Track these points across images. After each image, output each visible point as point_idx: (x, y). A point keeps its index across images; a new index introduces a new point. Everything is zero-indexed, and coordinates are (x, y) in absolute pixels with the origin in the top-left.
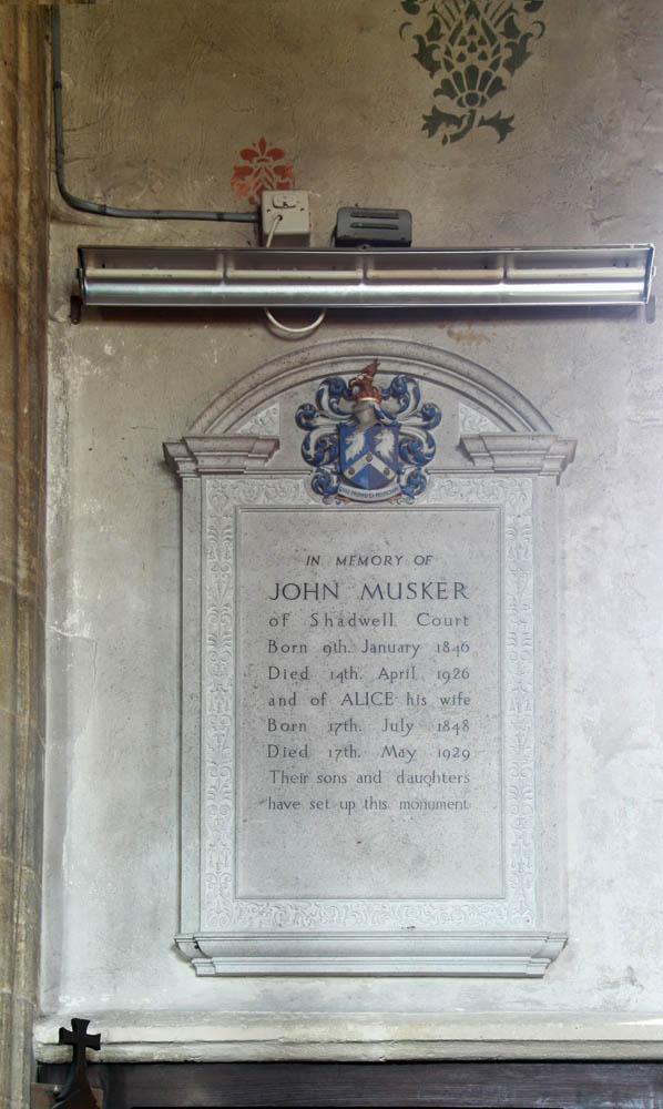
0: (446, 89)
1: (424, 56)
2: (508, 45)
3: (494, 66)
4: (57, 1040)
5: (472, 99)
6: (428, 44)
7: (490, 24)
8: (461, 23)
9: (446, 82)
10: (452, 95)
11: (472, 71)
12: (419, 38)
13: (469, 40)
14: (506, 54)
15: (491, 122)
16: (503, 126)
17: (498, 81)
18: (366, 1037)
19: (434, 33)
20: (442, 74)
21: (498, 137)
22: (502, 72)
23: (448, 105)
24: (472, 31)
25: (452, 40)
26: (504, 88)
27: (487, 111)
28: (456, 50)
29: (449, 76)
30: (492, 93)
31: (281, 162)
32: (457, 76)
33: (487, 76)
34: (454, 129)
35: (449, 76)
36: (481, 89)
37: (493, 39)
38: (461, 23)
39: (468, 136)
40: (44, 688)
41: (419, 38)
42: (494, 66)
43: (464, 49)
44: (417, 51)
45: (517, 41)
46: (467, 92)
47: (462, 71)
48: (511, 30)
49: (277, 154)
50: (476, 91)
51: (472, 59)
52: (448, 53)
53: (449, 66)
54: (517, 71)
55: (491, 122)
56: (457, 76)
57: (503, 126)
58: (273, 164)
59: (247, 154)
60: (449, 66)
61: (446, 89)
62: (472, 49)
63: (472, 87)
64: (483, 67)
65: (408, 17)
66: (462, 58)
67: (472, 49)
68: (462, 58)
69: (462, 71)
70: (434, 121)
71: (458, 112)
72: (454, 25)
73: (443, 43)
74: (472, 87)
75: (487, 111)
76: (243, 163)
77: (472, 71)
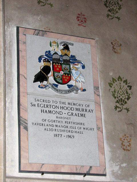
0: (117, 102)
2: (127, 95)
4: (20, 28)
6: (114, 93)
7: (124, 91)
8: (119, 90)
9: (109, 10)
11: (121, 99)
13: (120, 93)
14: (127, 97)
15: (117, 18)
17: (126, 101)
18: (81, 85)
19: (115, 92)
21: (127, 112)
23: (118, 105)
24: (121, 92)
25: (118, 93)
26: (127, 103)
27: (125, 107)
28: (110, 5)
31: (84, 17)
32: (119, 99)
33: (124, 100)
36: (115, 12)
38: (119, 90)
42: (125, 99)
43: (120, 95)
44: (112, 94)
45: (128, 95)
46: (113, 12)
47: (120, 99)
48: (127, 93)
49: (84, 15)
50: (122, 103)
51: (121, 97)
52: (117, 95)
54: (120, 10)
55: (117, 18)
56: (119, 99)
57: (119, 19)
58: (83, 17)
59: (79, 14)
60: (109, 7)
61: (117, 102)
62: (121, 95)
63: (122, 102)
64: (115, 8)
66: (111, 6)
69: (120, 99)
71: (120, 106)
72: (118, 90)
73: (116, 93)
74: (122, 102)
75: (116, 16)
76: (78, 16)
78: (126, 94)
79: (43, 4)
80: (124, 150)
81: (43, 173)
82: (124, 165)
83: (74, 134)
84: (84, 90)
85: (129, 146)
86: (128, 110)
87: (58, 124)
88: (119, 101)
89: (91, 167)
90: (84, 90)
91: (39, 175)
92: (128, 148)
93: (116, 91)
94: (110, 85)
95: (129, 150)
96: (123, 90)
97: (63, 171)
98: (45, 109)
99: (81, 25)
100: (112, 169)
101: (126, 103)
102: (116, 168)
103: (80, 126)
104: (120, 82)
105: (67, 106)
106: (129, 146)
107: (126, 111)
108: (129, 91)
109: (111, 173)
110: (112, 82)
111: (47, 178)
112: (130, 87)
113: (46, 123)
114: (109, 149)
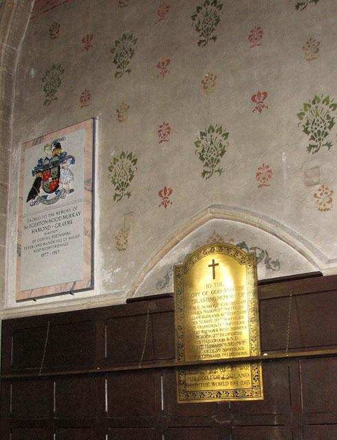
1: (306, 131)
3: (325, 128)
5: (213, 166)
9: (312, 136)
10: (314, 139)
11: (212, 159)
12: (200, 153)
15: (326, 144)
16: (220, 171)
17: (326, 132)
19: (308, 124)
20: (311, 134)
22: (327, 130)
28: (209, 154)
29: (313, 134)
30: (325, 136)
32: (315, 133)
34: (315, 149)
35: (313, 134)
37: (324, 121)
39: (211, 177)
40: (254, 325)
41: (200, 153)
42: (325, 128)
51: (318, 128)
53: (207, 159)
56: (315, 133)
60: (313, 132)
63: (319, 135)
64: (322, 130)
65: (197, 148)
67: (318, 125)
68: (316, 129)
70: (204, 173)
72: (313, 120)
77: (212, 159)
78: (128, 174)
79: (303, 6)
80: (119, 250)
81: (34, 299)
82: (118, 270)
83: (60, 248)
84: (72, 191)
85: (125, 243)
86: (129, 195)
87: (46, 241)
88: (316, 135)
89: (75, 283)
90: (72, 191)
91: (32, 302)
92: (125, 247)
93: (310, 122)
94: (110, 169)
95: (124, 249)
96: (321, 116)
97: (49, 293)
98: (35, 228)
99: (255, 45)
100: (103, 279)
101: (128, 185)
102: (108, 277)
103: (65, 236)
104: (128, 161)
105: (56, 216)
106: (125, 243)
107: (327, 147)
108: (133, 168)
109: (102, 283)
110: (330, 104)
111: (79, 297)
112: (135, 161)
113: (36, 243)
114: (102, 254)
